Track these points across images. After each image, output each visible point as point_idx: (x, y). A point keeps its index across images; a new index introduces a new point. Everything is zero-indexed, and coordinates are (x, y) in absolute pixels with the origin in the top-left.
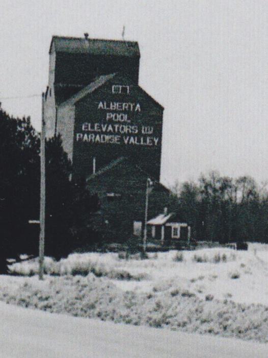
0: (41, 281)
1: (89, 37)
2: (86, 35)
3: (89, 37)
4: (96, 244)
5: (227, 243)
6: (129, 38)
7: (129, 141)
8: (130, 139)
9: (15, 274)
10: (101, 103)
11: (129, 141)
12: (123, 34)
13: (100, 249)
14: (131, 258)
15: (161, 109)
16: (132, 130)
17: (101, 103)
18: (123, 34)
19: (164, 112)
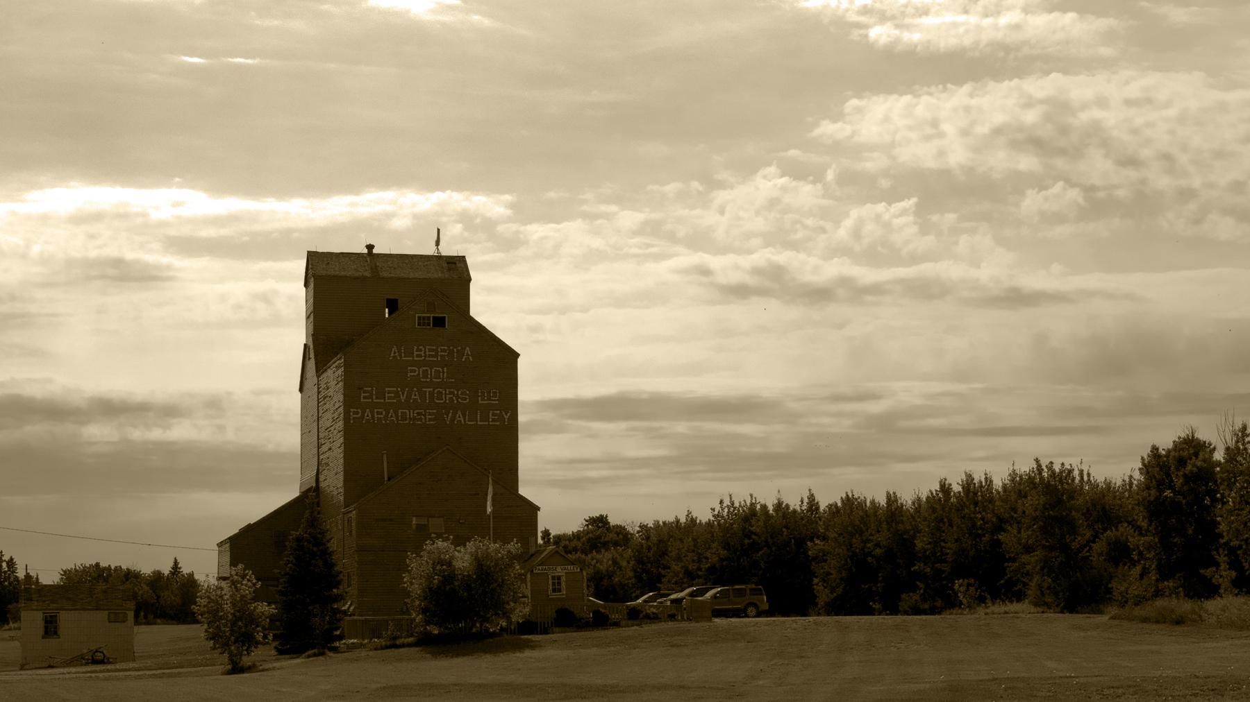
0: (752, 492)
1: (375, 251)
2: (370, 247)
3: (375, 251)
4: (192, 607)
5: (709, 567)
6: (447, 250)
7: (453, 419)
8: (455, 414)
9: (263, 670)
10: (395, 349)
11: (453, 419)
12: (438, 243)
13: (1129, 546)
14: (977, 95)
15: (511, 356)
16: (457, 396)
17: (395, 349)
18: (438, 243)
19: (520, 360)
